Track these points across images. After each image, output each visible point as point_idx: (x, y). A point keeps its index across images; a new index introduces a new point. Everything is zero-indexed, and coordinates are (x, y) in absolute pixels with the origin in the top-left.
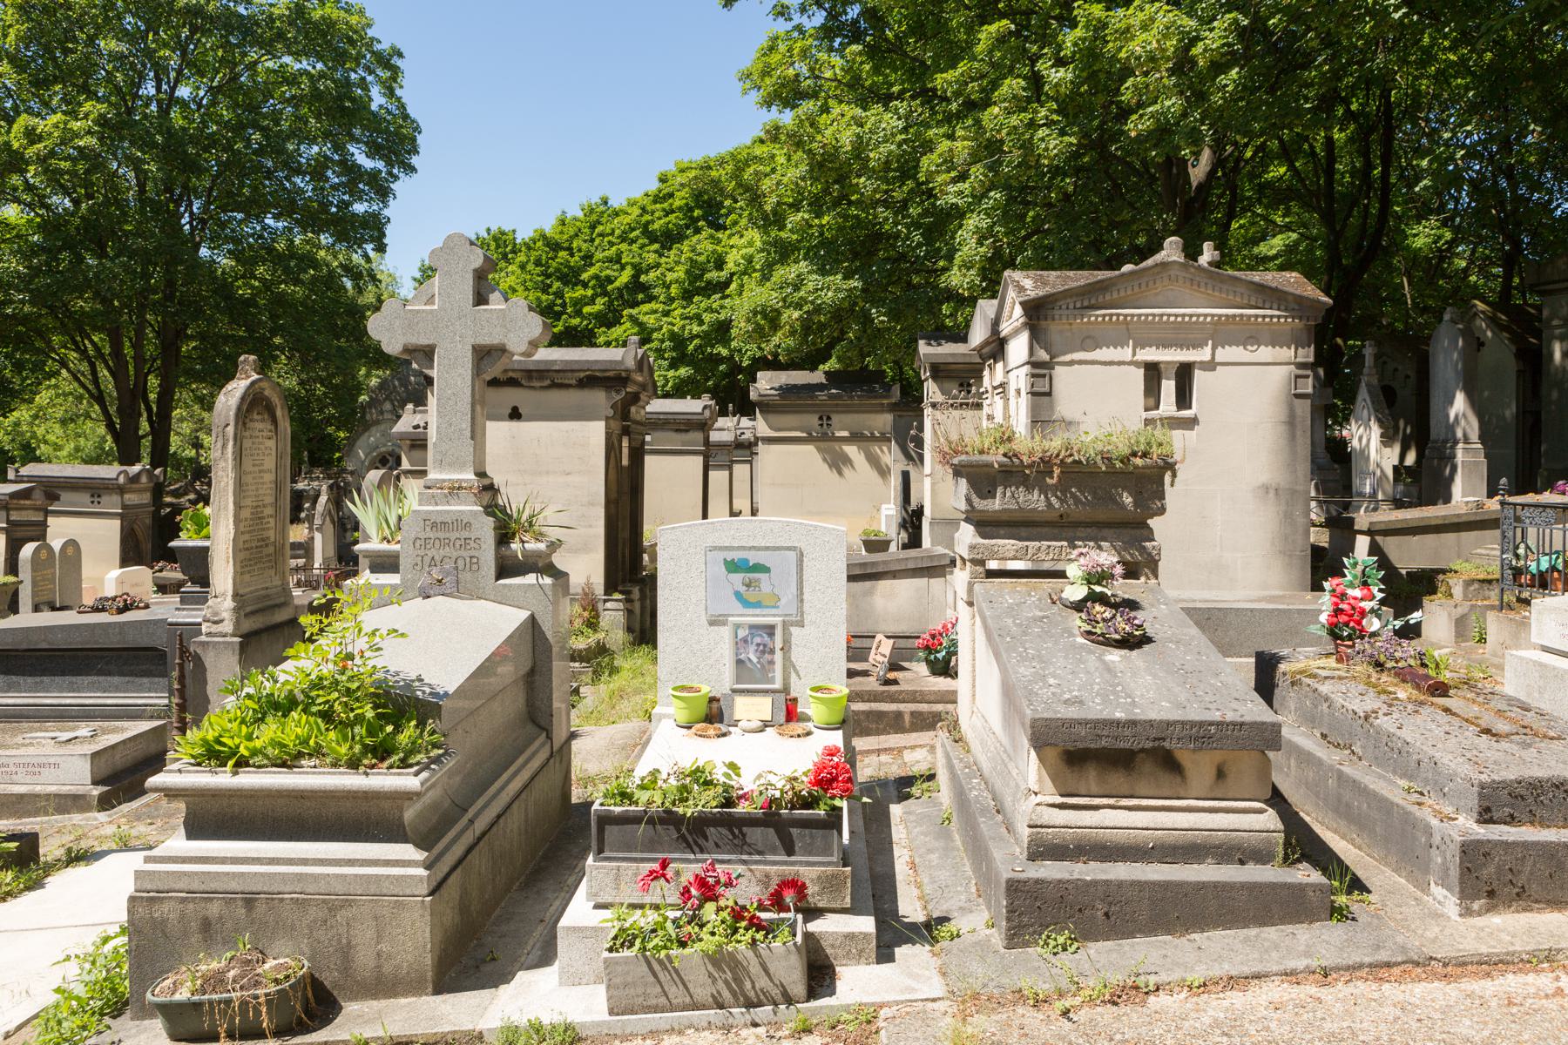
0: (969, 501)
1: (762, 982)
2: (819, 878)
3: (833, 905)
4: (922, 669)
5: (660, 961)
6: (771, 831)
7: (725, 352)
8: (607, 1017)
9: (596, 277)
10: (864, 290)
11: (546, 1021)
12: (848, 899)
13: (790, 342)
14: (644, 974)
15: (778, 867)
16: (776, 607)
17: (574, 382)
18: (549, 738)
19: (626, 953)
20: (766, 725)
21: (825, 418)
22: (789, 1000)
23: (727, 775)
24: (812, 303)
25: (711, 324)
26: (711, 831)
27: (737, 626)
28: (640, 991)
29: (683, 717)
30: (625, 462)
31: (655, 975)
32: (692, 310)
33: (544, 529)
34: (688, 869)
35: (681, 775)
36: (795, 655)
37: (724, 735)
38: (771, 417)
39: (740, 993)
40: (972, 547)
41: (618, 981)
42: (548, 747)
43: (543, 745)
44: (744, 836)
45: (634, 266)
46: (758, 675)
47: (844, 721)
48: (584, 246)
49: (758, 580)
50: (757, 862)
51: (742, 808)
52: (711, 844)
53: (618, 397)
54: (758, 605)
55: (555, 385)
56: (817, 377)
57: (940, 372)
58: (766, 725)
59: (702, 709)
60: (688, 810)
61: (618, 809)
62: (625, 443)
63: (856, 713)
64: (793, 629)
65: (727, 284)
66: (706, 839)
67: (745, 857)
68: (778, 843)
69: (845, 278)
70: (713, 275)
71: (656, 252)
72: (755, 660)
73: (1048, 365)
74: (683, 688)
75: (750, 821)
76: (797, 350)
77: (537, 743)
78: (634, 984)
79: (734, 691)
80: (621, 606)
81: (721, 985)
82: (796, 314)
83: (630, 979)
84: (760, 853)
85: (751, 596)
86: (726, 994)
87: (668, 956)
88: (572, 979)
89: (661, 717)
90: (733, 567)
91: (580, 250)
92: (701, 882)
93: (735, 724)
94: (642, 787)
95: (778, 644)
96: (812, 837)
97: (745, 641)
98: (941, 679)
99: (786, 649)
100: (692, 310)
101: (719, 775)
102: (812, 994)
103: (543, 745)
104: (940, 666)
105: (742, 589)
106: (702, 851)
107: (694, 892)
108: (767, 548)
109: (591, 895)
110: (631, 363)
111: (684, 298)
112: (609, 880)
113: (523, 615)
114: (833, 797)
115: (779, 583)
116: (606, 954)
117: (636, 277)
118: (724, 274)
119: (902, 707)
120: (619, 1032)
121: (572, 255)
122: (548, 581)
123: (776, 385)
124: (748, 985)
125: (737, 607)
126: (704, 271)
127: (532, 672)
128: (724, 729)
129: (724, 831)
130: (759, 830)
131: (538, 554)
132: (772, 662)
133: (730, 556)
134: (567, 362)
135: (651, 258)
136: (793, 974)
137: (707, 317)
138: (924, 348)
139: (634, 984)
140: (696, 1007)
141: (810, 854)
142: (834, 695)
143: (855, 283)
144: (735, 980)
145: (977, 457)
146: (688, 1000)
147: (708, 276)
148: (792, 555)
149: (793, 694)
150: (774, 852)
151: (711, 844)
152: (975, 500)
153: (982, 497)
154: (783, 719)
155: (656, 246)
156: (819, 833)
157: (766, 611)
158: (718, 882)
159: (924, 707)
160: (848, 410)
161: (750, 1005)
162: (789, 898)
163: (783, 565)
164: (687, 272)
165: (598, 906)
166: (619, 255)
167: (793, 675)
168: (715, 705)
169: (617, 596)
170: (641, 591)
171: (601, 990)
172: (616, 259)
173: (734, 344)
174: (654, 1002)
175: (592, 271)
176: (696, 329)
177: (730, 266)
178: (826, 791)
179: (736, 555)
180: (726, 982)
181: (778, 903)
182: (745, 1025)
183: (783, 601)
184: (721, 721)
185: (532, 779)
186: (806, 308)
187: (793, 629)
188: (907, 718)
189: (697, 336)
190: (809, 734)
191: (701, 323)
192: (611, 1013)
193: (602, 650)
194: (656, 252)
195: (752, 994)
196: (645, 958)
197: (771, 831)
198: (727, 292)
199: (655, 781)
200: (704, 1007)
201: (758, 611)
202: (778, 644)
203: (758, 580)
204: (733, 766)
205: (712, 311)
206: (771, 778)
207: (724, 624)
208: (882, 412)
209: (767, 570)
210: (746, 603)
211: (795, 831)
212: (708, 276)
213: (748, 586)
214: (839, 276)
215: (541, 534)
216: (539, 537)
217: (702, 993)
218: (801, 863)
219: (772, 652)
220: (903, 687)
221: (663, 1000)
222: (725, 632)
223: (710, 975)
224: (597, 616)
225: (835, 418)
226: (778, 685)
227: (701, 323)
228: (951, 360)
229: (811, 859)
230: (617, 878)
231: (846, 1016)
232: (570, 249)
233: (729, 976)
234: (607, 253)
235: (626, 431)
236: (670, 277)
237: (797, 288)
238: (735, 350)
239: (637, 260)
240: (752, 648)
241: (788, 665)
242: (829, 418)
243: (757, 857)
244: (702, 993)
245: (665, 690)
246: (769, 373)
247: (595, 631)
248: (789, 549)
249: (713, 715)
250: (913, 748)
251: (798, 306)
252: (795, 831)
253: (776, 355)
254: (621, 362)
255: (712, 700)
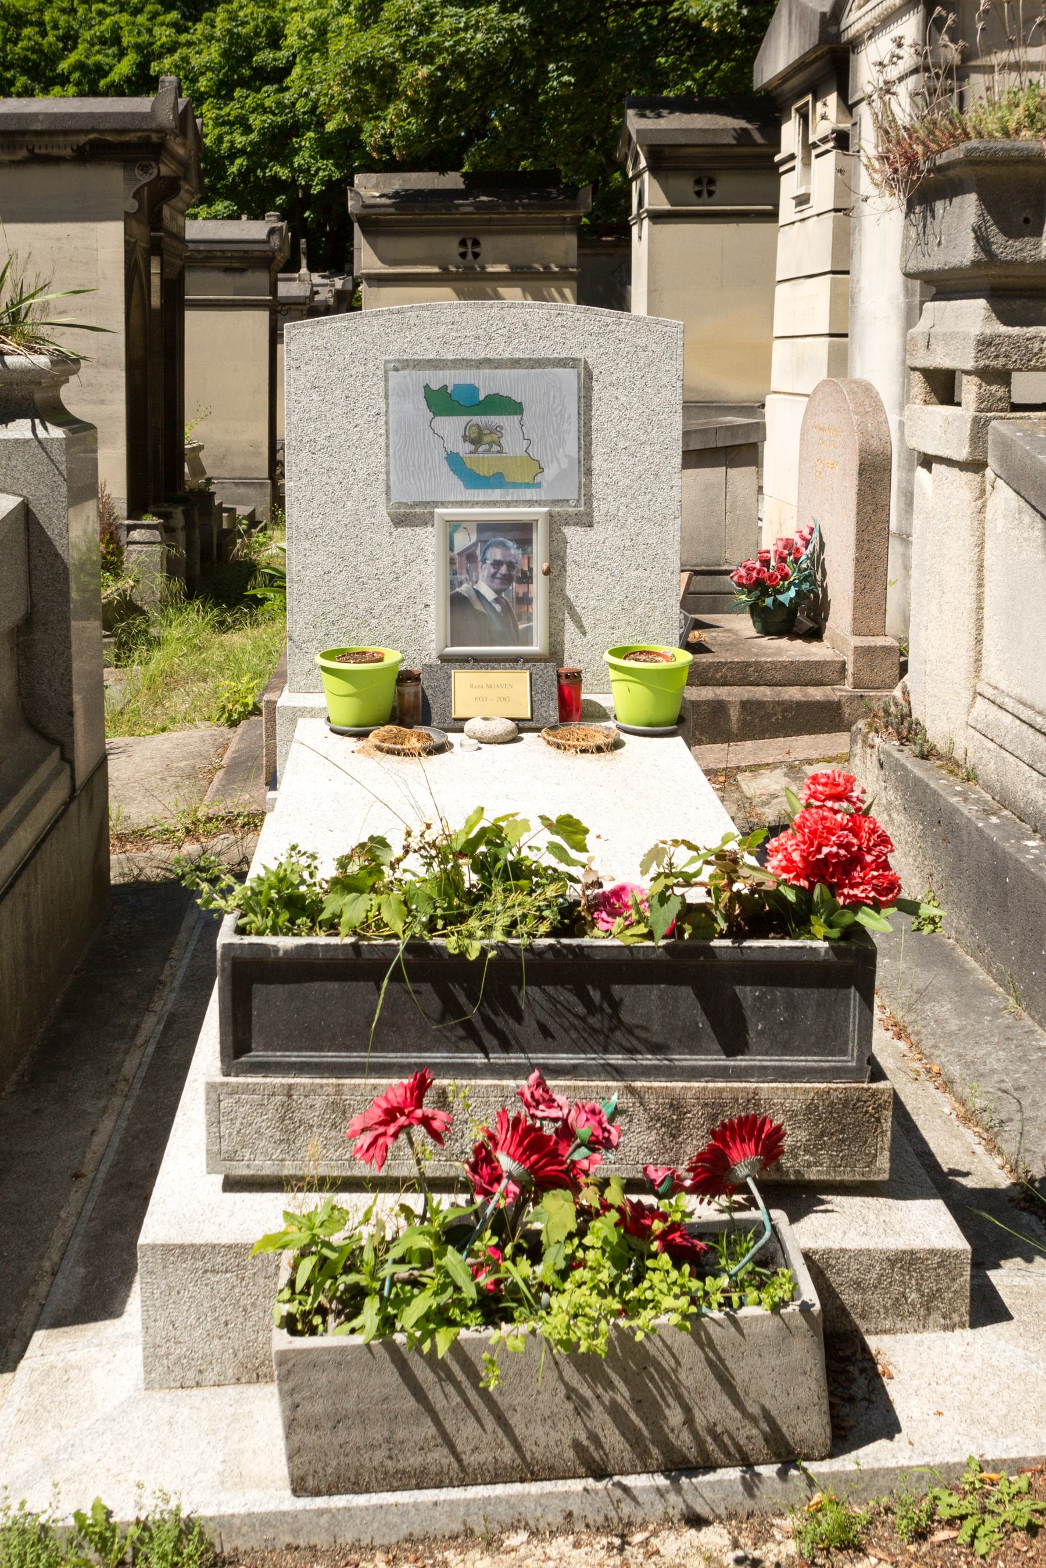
0: (982, 241)
1: (714, 1409)
2: (810, 1109)
3: (846, 1176)
4: (744, 625)
5: (431, 1359)
6: (686, 993)
7: (284, 173)
8: (287, 1502)
9: (80, 66)
10: (534, 32)
11: (124, 1514)
12: (884, 1161)
13: (413, 125)
14: (389, 1380)
15: (706, 1084)
16: (534, 485)
17: (68, 152)
18: (67, 759)
19: (335, 1337)
20: (521, 727)
21: (470, 245)
22: (788, 1456)
23: (555, 849)
24: (452, 50)
25: (262, 133)
26: (529, 995)
27: (453, 526)
28: (378, 1433)
29: (345, 712)
30: (156, 301)
31: (418, 1393)
32: (232, 110)
33: (44, 331)
34: (481, 1099)
35: (440, 853)
36: (578, 585)
37: (441, 749)
38: (383, 242)
39: (647, 1426)
40: (984, 343)
41: (318, 1408)
42: (64, 778)
43: (55, 775)
44: (616, 1005)
45: (139, 48)
46: (497, 626)
47: (680, 720)
48: (63, 20)
49: (497, 430)
50: (648, 1072)
51: (606, 936)
52: (530, 1025)
53: (146, 179)
54: (497, 481)
55: (36, 159)
56: (453, 180)
57: (664, 160)
58: (521, 727)
59: (385, 695)
60: (474, 940)
61: (285, 943)
62: (155, 269)
63: (696, 704)
64: (569, 531)
65: (287, 70)
66: (518, 1017)
67: (617, 1059)
68: (702, 1022)
69: (503, 10)
70: (265, 57)
71: (174, 25)
72: (490, 595)
73: (960, 72)
74: (343, 655)
75: (628, 967)
76: (419, 138)
77: (43, 771)
78: (362, 1418)
79: (446, 659)
80: (156, 535)
81: (600, 1418)
82: (424, 71)
83: (350, 1404)
84: (655, 1049)
85: (484, 463)
86: (613, 1439)
87: (456, 1347)
88: (171, 1369)
89: (296, 714)
90: (442, 402)
91: (56, 27)
92: (531, 1142)
93: (458, 725)
94: (344, 884)
95: (539, 562)
96: (792, 1006)
97: (469, 556)
98: (784, 642)
99: (555, 571)
100: (232, 110)
101: (535, 846)
102: (843, 1438)
103: (55, 775)
104: (780, 617)
105: (464, 449)
106: (506, 1046)
107: (506, 1162)
108: (516, 363)
109: (216, 1157)
110: (167, 118)
111: (218, 96)
112: (265, 1120)
113: (21, 499)
114: (856, 905)
115: (541, 435)
116: (282, 1340)
117: (143, 67)
118: (284, 54)
119: (723, 693)
120: (322, 1541)
121: (44, 34)
122: (57, 433)
123: (389, 191)
124: (674, 1416)
125: (455, 488)
126: (251, 53)
127: (26, 626)
128: (437, 738)
129: (565, 995)
130: (654, 993)
131: (33, 376)
132: (525, 600)
133: (437, 379)
134: (55, 116)
135: (163, 35)
136: (792, 1386)
137: (256, 121)
138: (634, 122)
139: (362, 1418)
140: (529, 1472)
141: (787, 1048)
142: (663, 665)
143: (519, 19)
144: (638, 1403)
145: (1002, 143)
146: (508, 1454)
147: (258, 58)
148: (569, 377)
149: (570, 664)
150: (693, 1046)
151: (530, 1025)
152: (998, 240)
153: (1011, 232)
154: (554, 715)
155: (174, 16)
156: (809, 997)
157: (512, 494)
158: (566, 1132)
159: (764, 693)
160: (508, 228)
161: (679, 1466)
162: (744, 1167)
163: (548, 396)
164: (225, 54)
165: (232, 1184)
166: (116, 29)
167: (570, 626)
168: (410, 689)
169: (149, 520)
170: (186, 514)
171: (264, 1408)
172: (114, 39)
173: (297, 161)
174: (414, 1461)
175: (73, 58)
176: (240, 140)
177: (292, 40)
178: (834, 889)
179: (451, 378)
180: (615, 1411)
181: (712, 1178)
182: (667, 1521)
183: (550, 473)
184: (427, 721)
185: (38, 846)
186: (439, 60)
187: (569, 531)
188: (734, 714)
189: (242, 152)
190: (617, 745)
191: (248, 130)
192: (299, 1487)
193: (128, 608)
194: (174, 25)
195: (684, 1440)
196: (391, 1348)
197: (686, 993)
198: (287, 82)
199: (376, 871)
200: (553, 1473)
201: (496, 494)
202: (539, 562)
203: (497, 430)
204: (570, 829)
205: (265, 111)
206: (681, 858)
207: (425, 521)
208: (562, 231)
209: (510, 406)
210: (472, 479)
211: (747, 994)
212: (258, 58)
213: (476, 441)
214: (494, 8)
215: (37, 339)
216: (32, 344)
217: (549, 1436)
218: (762, 1073)
219: (526, 578)
220: (721, 656)
221: (440, 1456)
222: (428, 540)
223: (571, 1393)
224: (118, 552)
225: (487, 244)
226: (537, 646)
227: (248, 130)
228: (683, 140)
229: (789, 1061)
230: (286, 1112)
231: (949, 1505)
232: (41, 24)
233: (622, 1393)
234: (97, 30)
235: (155, 248)
236: (196, 61)
237: (425, 30)
238: (300, 170)
239: (145, 37)
240: (485, 571)
241: (560, 605)
242: (476, 243)
243: (648, 1060)
244: (549, 1436)
245: (306, 660)
246: (373, 177)
247: (117, 576)
248: (562, 363)
249: (407, 711)
250: (755, 769)
251: (427, 58)
252: (747, 994)
253: (387, 149)
254: (151, 115)
255: (406, 678)
